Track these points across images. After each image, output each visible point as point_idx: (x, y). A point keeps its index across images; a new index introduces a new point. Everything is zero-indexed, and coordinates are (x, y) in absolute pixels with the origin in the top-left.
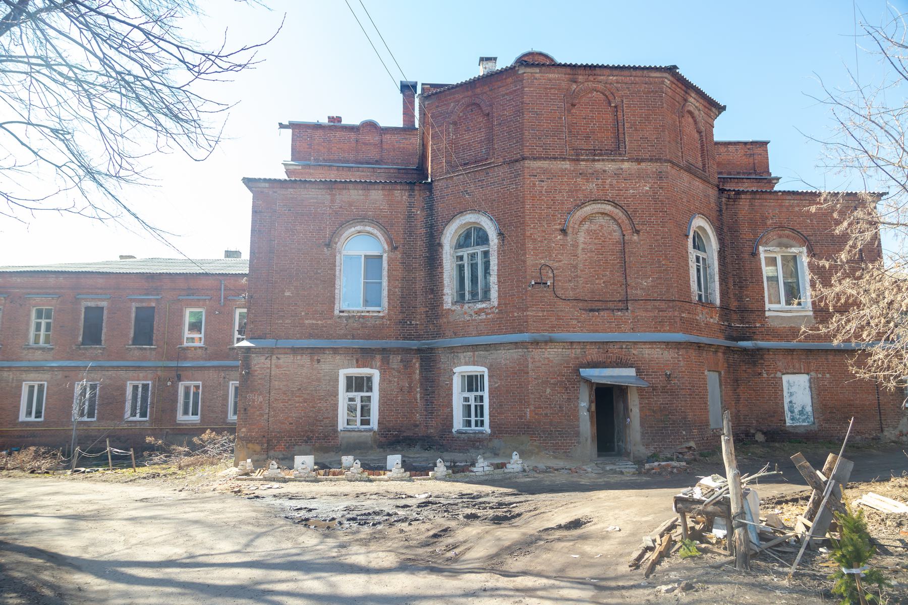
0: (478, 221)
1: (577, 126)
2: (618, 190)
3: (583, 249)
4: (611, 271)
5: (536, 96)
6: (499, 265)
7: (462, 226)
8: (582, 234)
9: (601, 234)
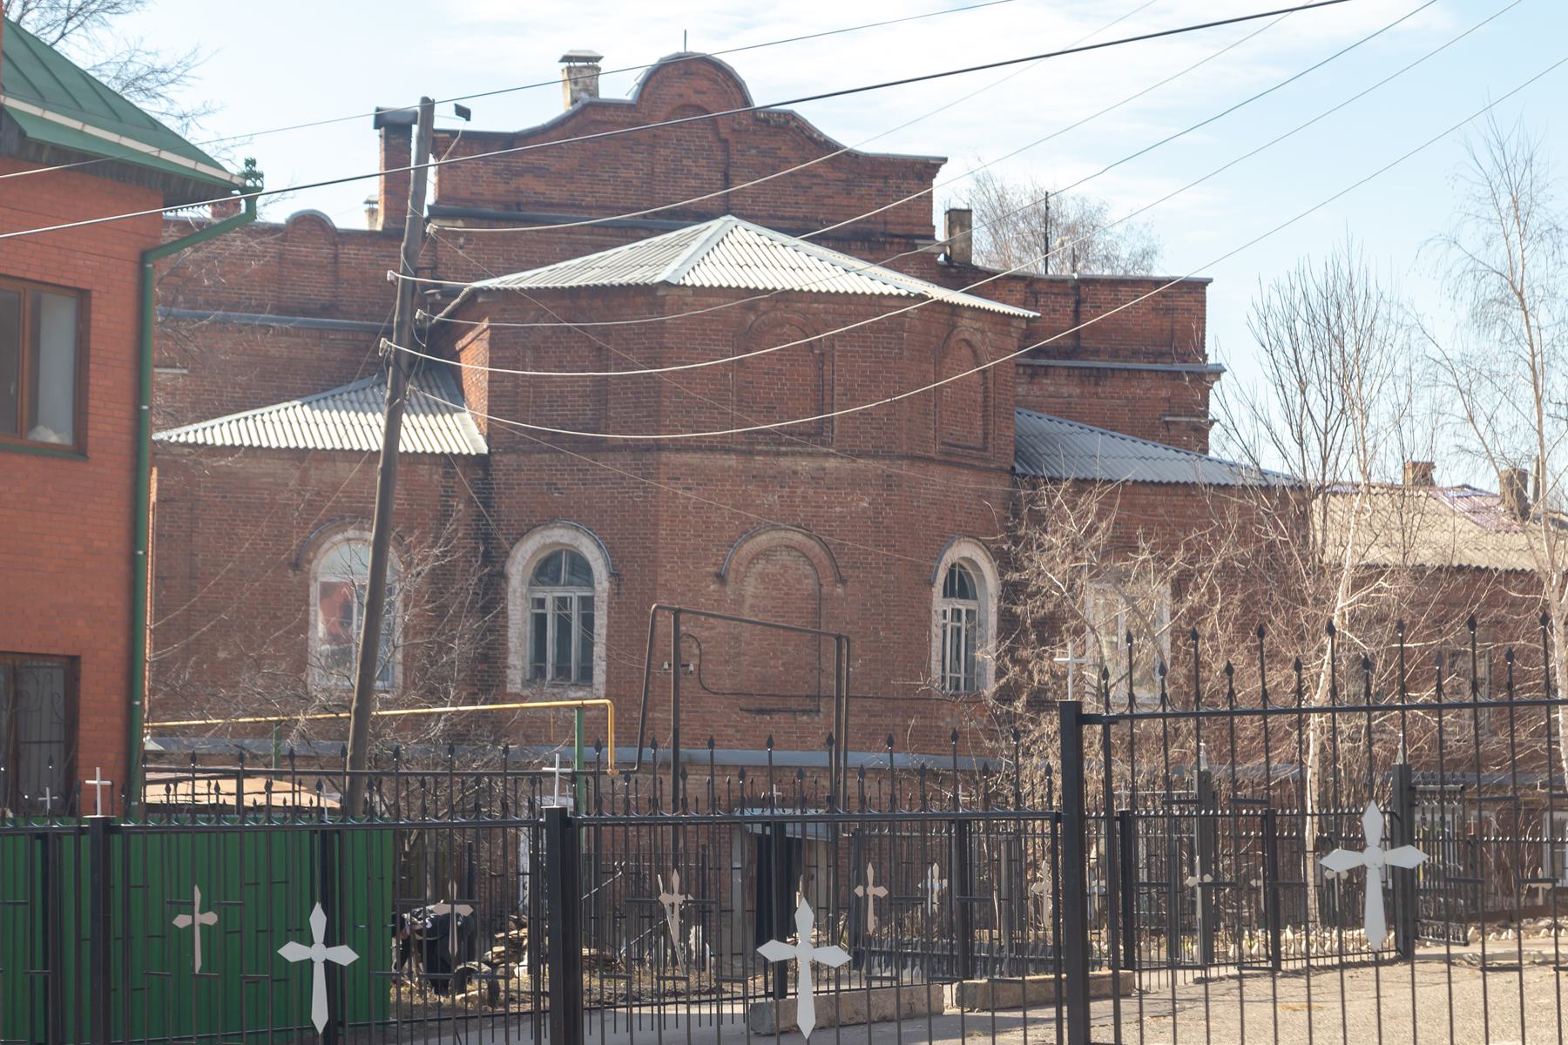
0: (576, 544)
1: (753, 387)
2: (816, 507)
3: (752, 606)
4: (796, 645)
5: (685, 334)
6: (609, 627)
7: (545, 546)
8: (752, 580)
9: (783, 581)
